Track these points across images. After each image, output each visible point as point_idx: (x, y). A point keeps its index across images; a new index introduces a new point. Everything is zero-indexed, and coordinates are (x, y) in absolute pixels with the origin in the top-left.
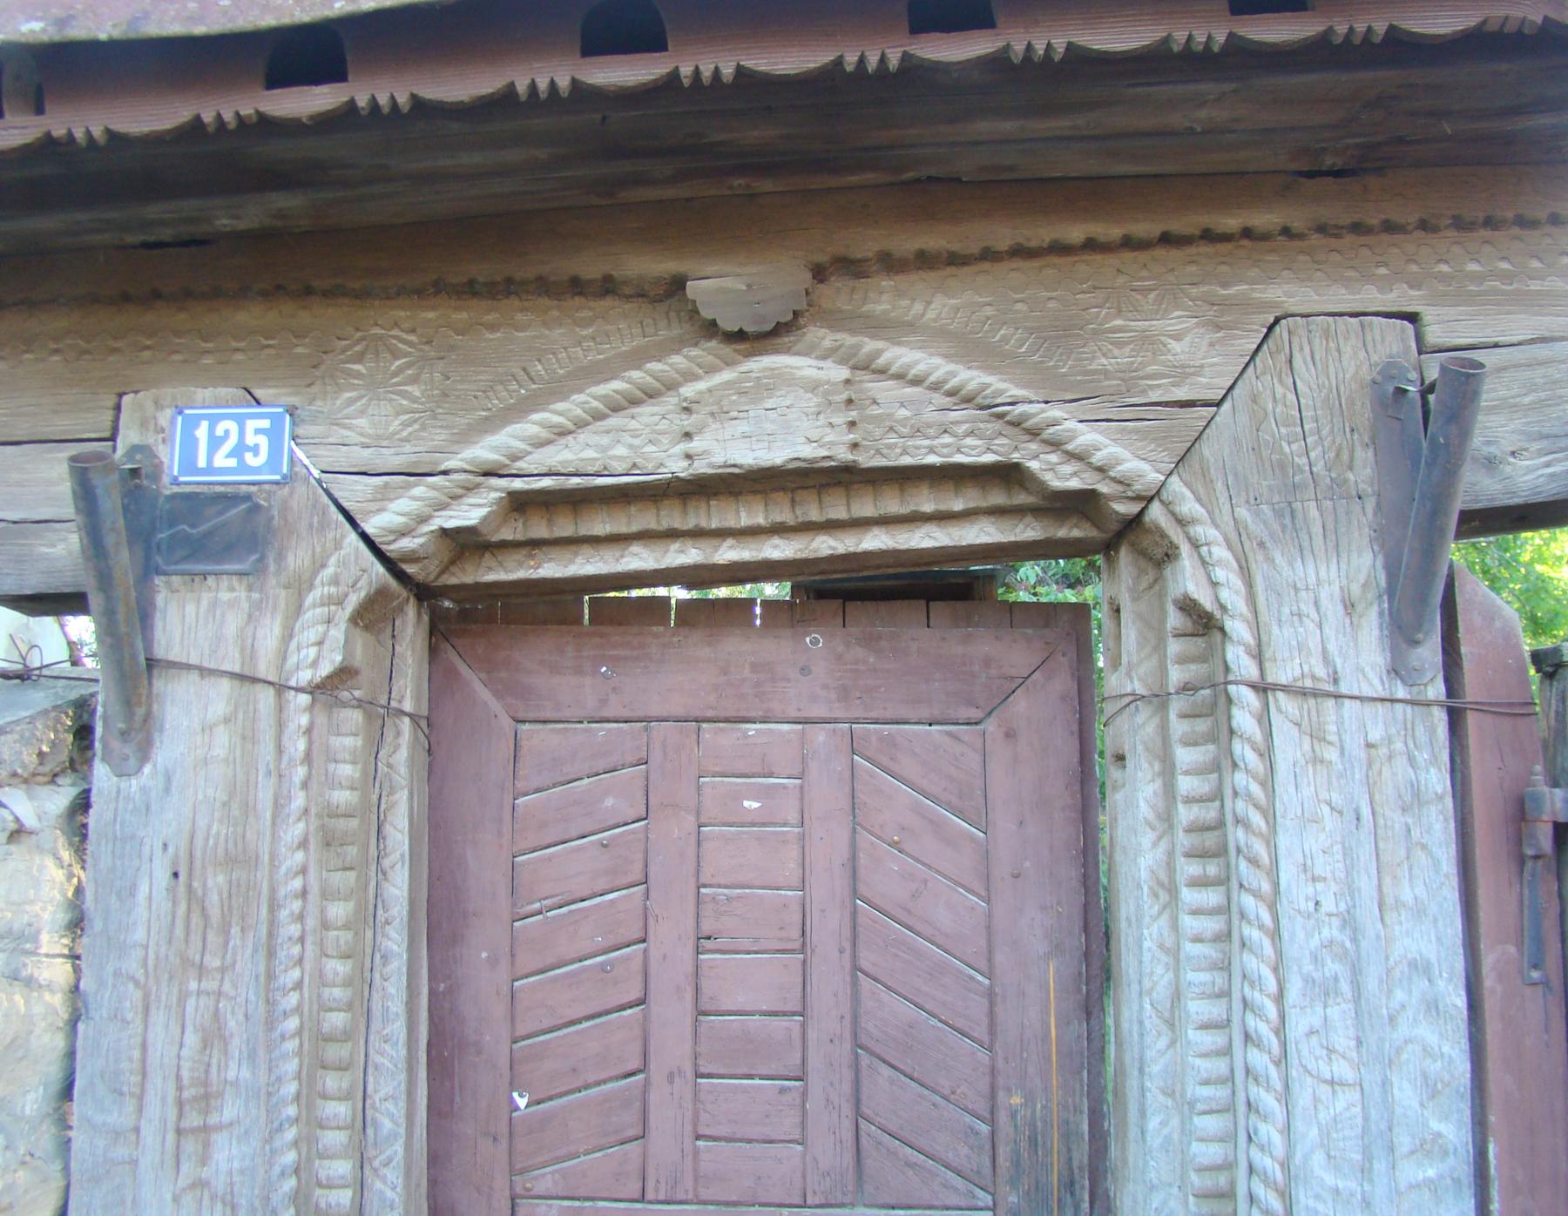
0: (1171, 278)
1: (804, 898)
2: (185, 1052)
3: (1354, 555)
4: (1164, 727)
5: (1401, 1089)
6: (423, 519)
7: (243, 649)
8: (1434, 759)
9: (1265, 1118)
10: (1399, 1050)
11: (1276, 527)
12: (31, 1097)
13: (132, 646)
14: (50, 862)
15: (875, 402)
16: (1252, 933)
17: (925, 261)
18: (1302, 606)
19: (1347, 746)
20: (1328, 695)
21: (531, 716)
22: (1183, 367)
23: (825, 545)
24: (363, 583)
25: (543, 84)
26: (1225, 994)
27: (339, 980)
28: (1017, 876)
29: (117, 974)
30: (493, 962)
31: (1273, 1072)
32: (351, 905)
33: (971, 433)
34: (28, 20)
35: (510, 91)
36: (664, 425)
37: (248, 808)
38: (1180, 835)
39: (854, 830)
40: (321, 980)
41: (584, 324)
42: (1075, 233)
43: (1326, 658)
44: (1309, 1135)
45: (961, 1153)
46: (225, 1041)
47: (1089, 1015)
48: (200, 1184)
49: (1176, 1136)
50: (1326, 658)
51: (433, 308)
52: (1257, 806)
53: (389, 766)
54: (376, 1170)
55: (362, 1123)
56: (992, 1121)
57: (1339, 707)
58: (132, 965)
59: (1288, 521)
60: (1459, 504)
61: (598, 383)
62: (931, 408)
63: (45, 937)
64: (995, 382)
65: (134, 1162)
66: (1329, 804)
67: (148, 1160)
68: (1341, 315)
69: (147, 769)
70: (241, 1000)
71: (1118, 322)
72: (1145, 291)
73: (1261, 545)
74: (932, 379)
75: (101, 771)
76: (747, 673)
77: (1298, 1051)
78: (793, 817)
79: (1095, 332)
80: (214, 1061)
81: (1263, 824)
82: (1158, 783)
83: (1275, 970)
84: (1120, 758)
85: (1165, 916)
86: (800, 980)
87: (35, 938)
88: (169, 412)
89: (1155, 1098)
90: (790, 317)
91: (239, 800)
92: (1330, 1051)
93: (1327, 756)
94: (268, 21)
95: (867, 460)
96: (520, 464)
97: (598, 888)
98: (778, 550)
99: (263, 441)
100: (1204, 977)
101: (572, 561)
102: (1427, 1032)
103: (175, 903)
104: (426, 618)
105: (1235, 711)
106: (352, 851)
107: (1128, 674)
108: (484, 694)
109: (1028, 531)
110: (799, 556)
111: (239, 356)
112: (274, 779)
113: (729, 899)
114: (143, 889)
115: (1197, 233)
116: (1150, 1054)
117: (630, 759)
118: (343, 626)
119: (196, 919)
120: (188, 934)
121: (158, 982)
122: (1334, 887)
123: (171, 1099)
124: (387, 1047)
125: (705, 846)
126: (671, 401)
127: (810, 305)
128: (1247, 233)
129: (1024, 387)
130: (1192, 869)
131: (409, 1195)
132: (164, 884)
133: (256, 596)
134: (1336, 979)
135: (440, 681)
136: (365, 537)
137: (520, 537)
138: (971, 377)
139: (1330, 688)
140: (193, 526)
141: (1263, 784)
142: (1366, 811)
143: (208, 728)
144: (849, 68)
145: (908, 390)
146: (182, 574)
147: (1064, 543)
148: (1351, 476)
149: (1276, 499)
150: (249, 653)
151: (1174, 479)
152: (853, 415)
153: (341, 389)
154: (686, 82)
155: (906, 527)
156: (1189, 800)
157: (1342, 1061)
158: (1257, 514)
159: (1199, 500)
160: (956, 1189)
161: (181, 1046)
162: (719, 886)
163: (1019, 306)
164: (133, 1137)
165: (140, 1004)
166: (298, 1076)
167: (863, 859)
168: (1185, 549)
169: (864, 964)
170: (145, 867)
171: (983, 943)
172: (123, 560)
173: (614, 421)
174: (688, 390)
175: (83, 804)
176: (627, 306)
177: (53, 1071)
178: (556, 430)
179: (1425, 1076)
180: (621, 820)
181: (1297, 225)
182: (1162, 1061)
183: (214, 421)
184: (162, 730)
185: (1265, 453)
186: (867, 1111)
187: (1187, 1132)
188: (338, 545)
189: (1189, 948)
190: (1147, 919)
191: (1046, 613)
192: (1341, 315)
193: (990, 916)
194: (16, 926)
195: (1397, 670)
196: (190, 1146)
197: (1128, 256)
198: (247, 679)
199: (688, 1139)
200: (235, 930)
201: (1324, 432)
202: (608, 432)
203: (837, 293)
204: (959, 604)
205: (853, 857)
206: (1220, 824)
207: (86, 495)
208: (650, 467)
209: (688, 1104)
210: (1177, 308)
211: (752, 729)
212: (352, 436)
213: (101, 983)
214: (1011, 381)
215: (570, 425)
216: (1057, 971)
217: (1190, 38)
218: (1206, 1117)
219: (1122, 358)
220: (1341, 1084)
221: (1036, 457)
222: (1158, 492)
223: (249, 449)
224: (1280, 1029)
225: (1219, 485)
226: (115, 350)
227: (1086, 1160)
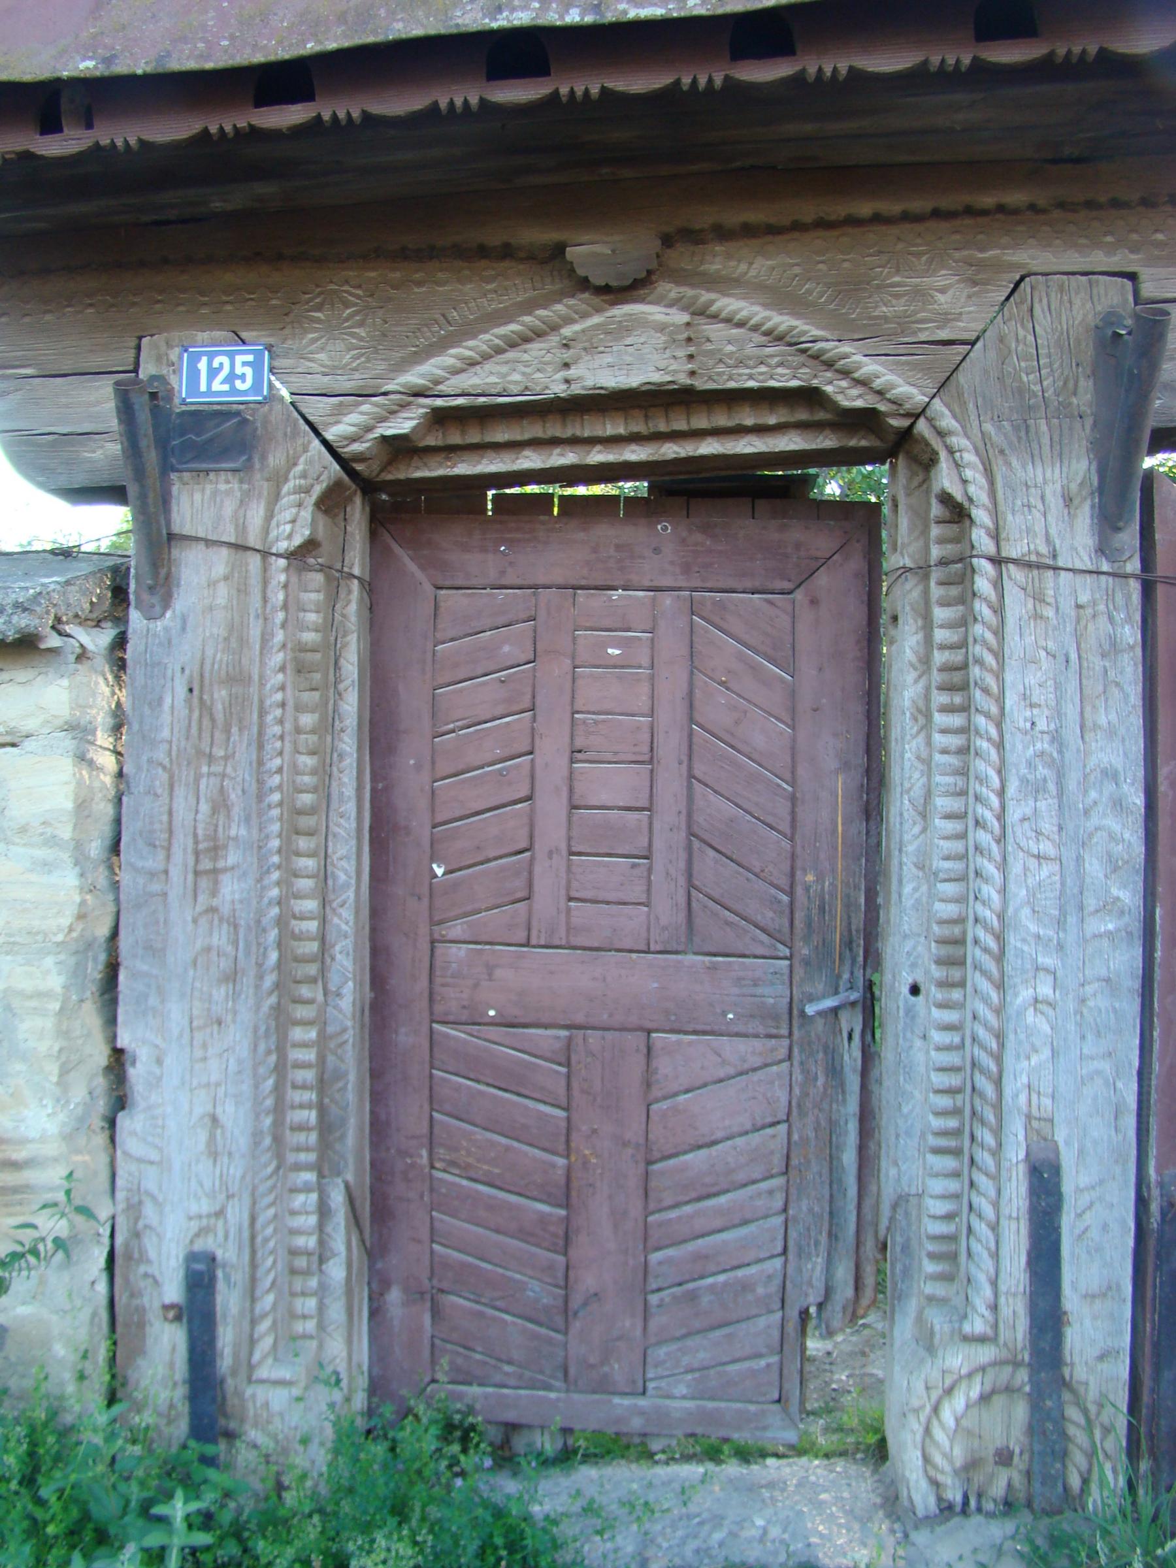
2: (200, 817)
3: (1074, 461)
4: (926, 593)
6: (369, 429)
7: (237, 526)
9: (986, 881)
10: (1091, 836)
11: (1015, 440)
12: (94, 844)
13: (158, 522)
14: (101, 680)
15: (709, 340)
16: (984, 745)
17: (748, 231)
19: (1061, 606)
20: (1049, 567)
21: (448, 583)
23: (671, 451)
25: (459, 102)
26: (963, 793)
27: (307, 770)
28: (815, 710)
29: (150, 761)
30: (418, 767)
31: (995, 848)
32: (316, 716)
33: (781, 364)
34: (83, 60)
35: (435, 107)
36: (548, 358)
37: (243, 642)
39: (692, 673)
40: (296, 770)
42: (865, 209)
43: (1048, 539)
44: (1019, 893)
45: (767, 916)
48: (212, 910)
49: (924, 900)
50: (1048, 539)
51: (373, 269)
52: (990, 649)
53: (344, 616)
55: (324, 876)
56: (791, 893)
57: (1057, 577)
58: (161, 755)
59: (1023, 434)
63: (99, 734)
64: (800, 325)
65: (165, 894)
66: (1045, 649)
67: (174, 894)
69: (168, 614)
70: (239, 779)
71: (897, 279)
72: (918, 255)
73: (1002, 452)
74: (752, 322)
75: (134, 615)
76: (612, 552)
78: (645, 661)
79: (879, 287)
83: (999, 772)
84: (895, 619)
85: (923, 735)
86: (648, 784)
87: (93, 732)
88: (177, 350)
89: (909, 870)
90: (644, 274)
91: (236, 635)
92: (1038, 833)
93: (1045, 614)
94: (259, 58)
95: (701, 384)
96: (440, 387)
97: (497, 713)
98: (635, 454)
99: (249, 371)
100: (949, 779)
101: (479, 463)
102: (1113, 824)
103: (191, 710)
105: (977, 578)
106: (317, 676)
107: (902, 554)
108: (412, 567)
109: (827, 441)
110: (651, 458)
111: (229, 307)
112: (261, 621)
113: (596, 722)
114: (168, 701)
115: (960, 208)
116: (906, 837)
117: (523, 616)
118: (310, 509)
119: (206, 722)
121: (179, 765)
122: (1046, 712)
123: (190, 850)
124: (342, 821)
125: (579, 682)
126: (554, 339)
127: (660, 265)
128: (1001, 209)
129: (823, 329)
130: (942, 698)
133: (245, 486)
134: (1045, 780)
136: (325, 443)
137: (440, 443)
138: (782, 321)
139: (1050, 562)
140: (198, 435)
141: (995, 633)
142: (1073, 656)
143: (212, 584)
144: (685, 88)
145: (734, 331)
146: (191, 471)
147: (855, 450)
148: (1074, 400)
149: (1015, 417)
150: (242, 529)
151: (937, 401)
152: (692, 349)
153: (306, 331)
154: (564, 99)
155: (732, 437)
156: (942, 647)
157: (1047, 842)
158: (999, 428)
159: (955, 417)
160: (762, 943)
161: (197, 812)
162: (589, 713)
163: (821, 266)
164: (163, 877)
166: (280, 836)
167: (698, 693)
168: (943, 455)
169: (697, 773)
170: (169, 684)
172: (152, 457)
173: (511, 355)
174: (567, 331)
175: (121, 642)
176: (521, 267)
180: (515, 662)
181: (1041, 202)
182: (916, 843)
183: (211, 356)
184: (178, 586)
185: (1008, 381)
186: (697, 883)
187: (932, 896)
188: (306, 450)
189: (938, 757)
190: (908, 737)
191: (843, 509)
193: (794, 740)
194: (83, 722)
195: (1103, 549)
196: (204, 883)
198: (239, 547)
199: (563, 900)
200: (235, 730)
201: (1055, 366)
203: (681, 257)
205: (691, 694)
206: (964, 666)
207: (126, 410)
208: (538, 389)
209: (563, 875)
210: (943, 267)
211: (616, 595)
214: (813, 324)
215: (479, 359)
216: (844, 783)
217: (943, 61)
218: (947, 884)
219: (899, 306)
220: (1046, 858)
221: (830, 383)
222: (924, 410)
223: (238, 377)
224: (1001, 816)
225: (971, 406)
226: (134, 304)
227: (862, 926)
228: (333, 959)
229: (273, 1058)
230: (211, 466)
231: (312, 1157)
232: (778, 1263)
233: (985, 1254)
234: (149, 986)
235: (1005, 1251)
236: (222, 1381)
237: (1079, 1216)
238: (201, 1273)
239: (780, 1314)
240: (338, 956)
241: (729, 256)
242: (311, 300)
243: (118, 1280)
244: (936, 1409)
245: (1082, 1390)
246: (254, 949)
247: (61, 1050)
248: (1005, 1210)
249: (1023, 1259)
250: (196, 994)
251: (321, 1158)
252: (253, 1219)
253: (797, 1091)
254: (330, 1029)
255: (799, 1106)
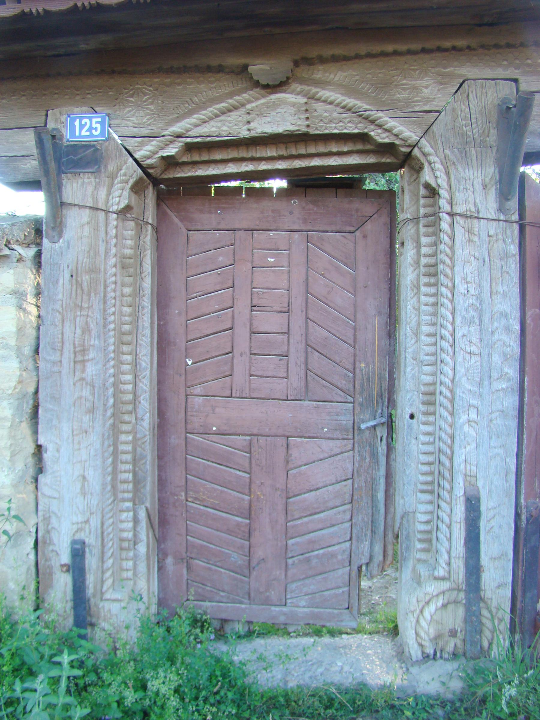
0: (425, 65)
1: (289, 293)
2: (76, 335)
3: (488, 168)
4: (418, 230)
5: (495, 357)
7: (93, 199)
8: (513, 242)
10: (495, 343)
12: (26, 348)
15: (316, 111)
17: (335, 59)
18: (468, 186)
20: (476, 218)
21: (193, 228)
22: (428, 98)
23: (298, 164)
24: (135, 176)
26: (435, 324)
27: (127, 314)
30: (180, 314)
31: (450, 349)
32: (131, 289)
33: (350, 122)
36: (240, 119)
37: (96, 253)
38: (422, 268)
39: (308, 270)
40: (122, 314)
41: (212, 83)
42: (390, 48)
44: (461, 370)
45: (343, 383)
46: (90, 332)
47: (390, 337)
48: (82, 379)
49: (416, 374)
52: (448, 256)
53: (144, 242)
54: (140, 380)
55: (135, 364)
56: (354, 373)
57: (479, 222)
58: (58, 307)
59: (464, 155)
60: (525, 149)
61: (217, 104)
62: (336, 113)
63: (29, 296)
64: (359, 103)
66: (474, 256)
67: (65, 371)
68: (488, 79)
69: (61, 241)
70: (95, 318)
71: (405, 82)
72: (415, 70)
73: (454, 163)
74: (336, 102)
76: (270, 213)
77: (459, 342)
78: (286, 264)
79: (396, 85)
80: (86, 338)
81: (450, 262)
82: (415, 250)
83: (452, 314)
85: (416, 297)
87: (26, 295)
88: (65, 116)
89: (410, 360)
90: (285, 79)
91: (93, 251)
92: (470, 342)
93: (474, 239)
95: (312, 131)
96: (189, 133)
97: (216, 289)
98: (281, 165)
99: (99, 126)
100: (428, 318)
101: (208, 170)
103: (72, 286)
104: (156, 193)
105: (442, 223)
106: (132, 270)
108: (176, 220)
109: (371, 159)
110: (289, 167)
111: (89, 96)
112: (105, 243)
113: (263, 293)
114: (61, 281)
116: (408, 345)
117: (229, 243)
118: (128, 190)
119: (79, 291)
120: (76, 296)
121: (66, 311)
122: (474, 286)
123: (72, 351)
124: (144, 338)
125: (255, 274)
126: (243, 110)
127: (293, 75)
128: (454, 48)
129: (370, 105)
130: (425, 280)
131: (151, 390)
132: (68, 279)
133: (97, 180)
134: (473, 317)
135: (161, 216)
136: (136, 160)
137: (189, 160)
138: (350, 101)
140: (75, 156)
141: (450, 249)
142: (487, 259)
143: (82, 226)
148: (488, 139)
149: (460, 147)
150: (96, 200)
151: (423, 139)
152: (308, 115)
153: (126, 107)
155: (327, 157)
156: (425, 256)
159: (432, 147)
161: (75, 333)
163: (369, 76)
165: (61, 320)
166: (114, 344)
167: (310, 279)
168: (426, 165)
169: (310, 316)
170: (62, 273)
171: (352, 310)
172: (53, 165)
173: (223, 118)
174: (249, 106)
175: (39, 255)
176: (227, 76)
177: (33, 342)
179: (503, 352)
180: (225, 265)
181: (473, 45)
183: (81, 119)
184: (66, 227)
186: (310, 368)
188: (126, 163)
189: (423, 308)
190: (409, 298)
192: (488, 79)
193: (355, 301)
196: (78, 366)
197: (409, 57)
198: (95, 209)
199: (247, 376)
200: (93, 294)
201: (479, 123)
202: (220, 121)
203: (303, 71)
204: (348, 190)
205: (307, 279)
207: (40, 143)
208: (235, 134)
211: (271, 233)
212: (130, 124)
213: (48, 313)
214: (365, 103)
216: (379, 321)
219: (406, 95)
220: (473, 354)
222: (417, 144)
223: (94, 129)
224: (453, 334)
225: (439, 141)
226: (44, 95)
228: (140, 403)
229: (112, 448)
230: (81, 171)
231: (130, 495)
232: (348, 544)
233: (445, 539)
234: (53, 415)
235: (454, 538)
236: (89, 600)
237: (488, 521)
238: (78, 550)
239: (349, 568)
240: (142, 401)
241: (325, 71)
243: (40, 553)
244: (421, 611)
245: (489, 602)
246: (102, 397)
247: (11, 445)
248: (454, 519)
249: (463, 541)
250: (75, 419)
251: (134, 496)
252: (103, 524)
253: (356, 464)
254: (138, 436)
255: (358, 471)
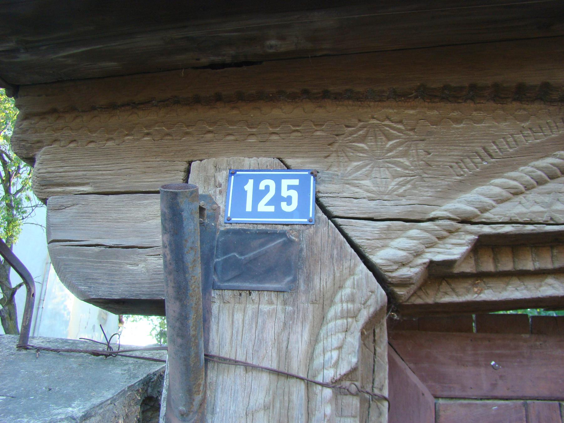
6: (418, 254)
7: (279, 351)
13: (197, 346)
21: (446, 394)
24: (371, 301)
41: (526, 119)
51: (413, 108)
61: (537, 159)
96: (487, 215)
99: (294, 194)
101: (505, 290)
111: (274, 137)
118: (358, 335)
133: (289, 308)
140: (242, 254)
153: (350, 160)
173: (551, 186)
176: (551, 108)
178: (513, 191)
184: (213, 412)
188: (352, 273)
202: (549, 193)
212: (361, 192)
215: (523, 189)
223: (284, 199)
226: (187, 133)
230: (254, 286)
242: (356, 132)
